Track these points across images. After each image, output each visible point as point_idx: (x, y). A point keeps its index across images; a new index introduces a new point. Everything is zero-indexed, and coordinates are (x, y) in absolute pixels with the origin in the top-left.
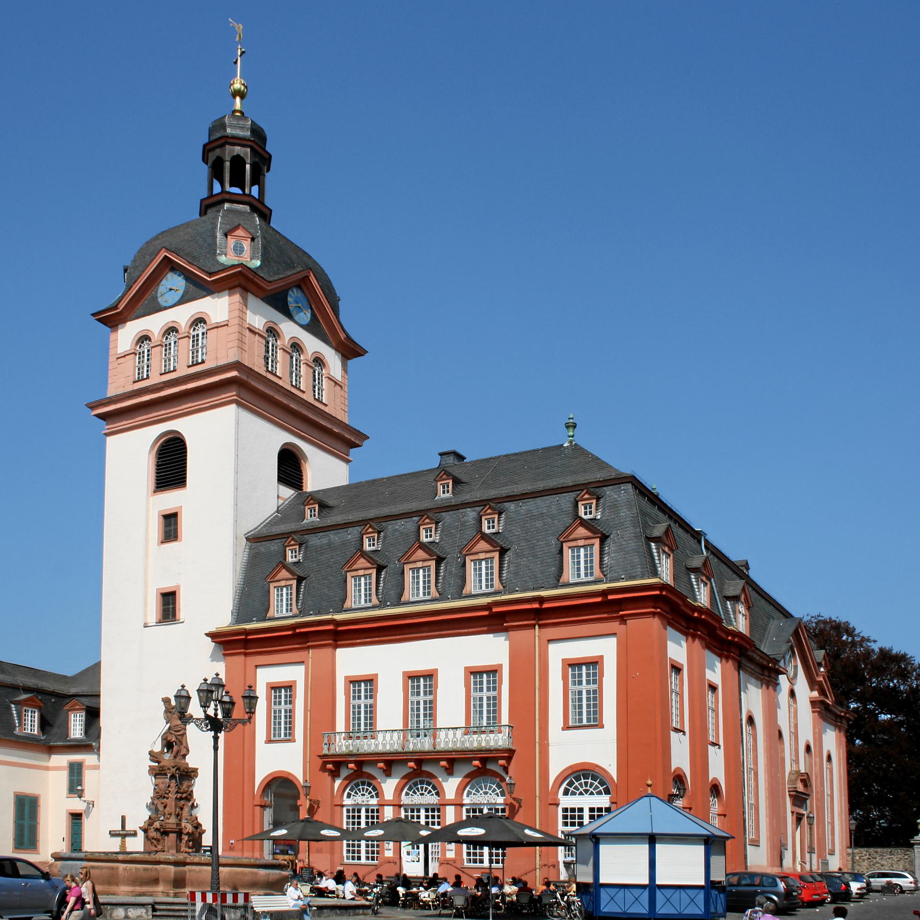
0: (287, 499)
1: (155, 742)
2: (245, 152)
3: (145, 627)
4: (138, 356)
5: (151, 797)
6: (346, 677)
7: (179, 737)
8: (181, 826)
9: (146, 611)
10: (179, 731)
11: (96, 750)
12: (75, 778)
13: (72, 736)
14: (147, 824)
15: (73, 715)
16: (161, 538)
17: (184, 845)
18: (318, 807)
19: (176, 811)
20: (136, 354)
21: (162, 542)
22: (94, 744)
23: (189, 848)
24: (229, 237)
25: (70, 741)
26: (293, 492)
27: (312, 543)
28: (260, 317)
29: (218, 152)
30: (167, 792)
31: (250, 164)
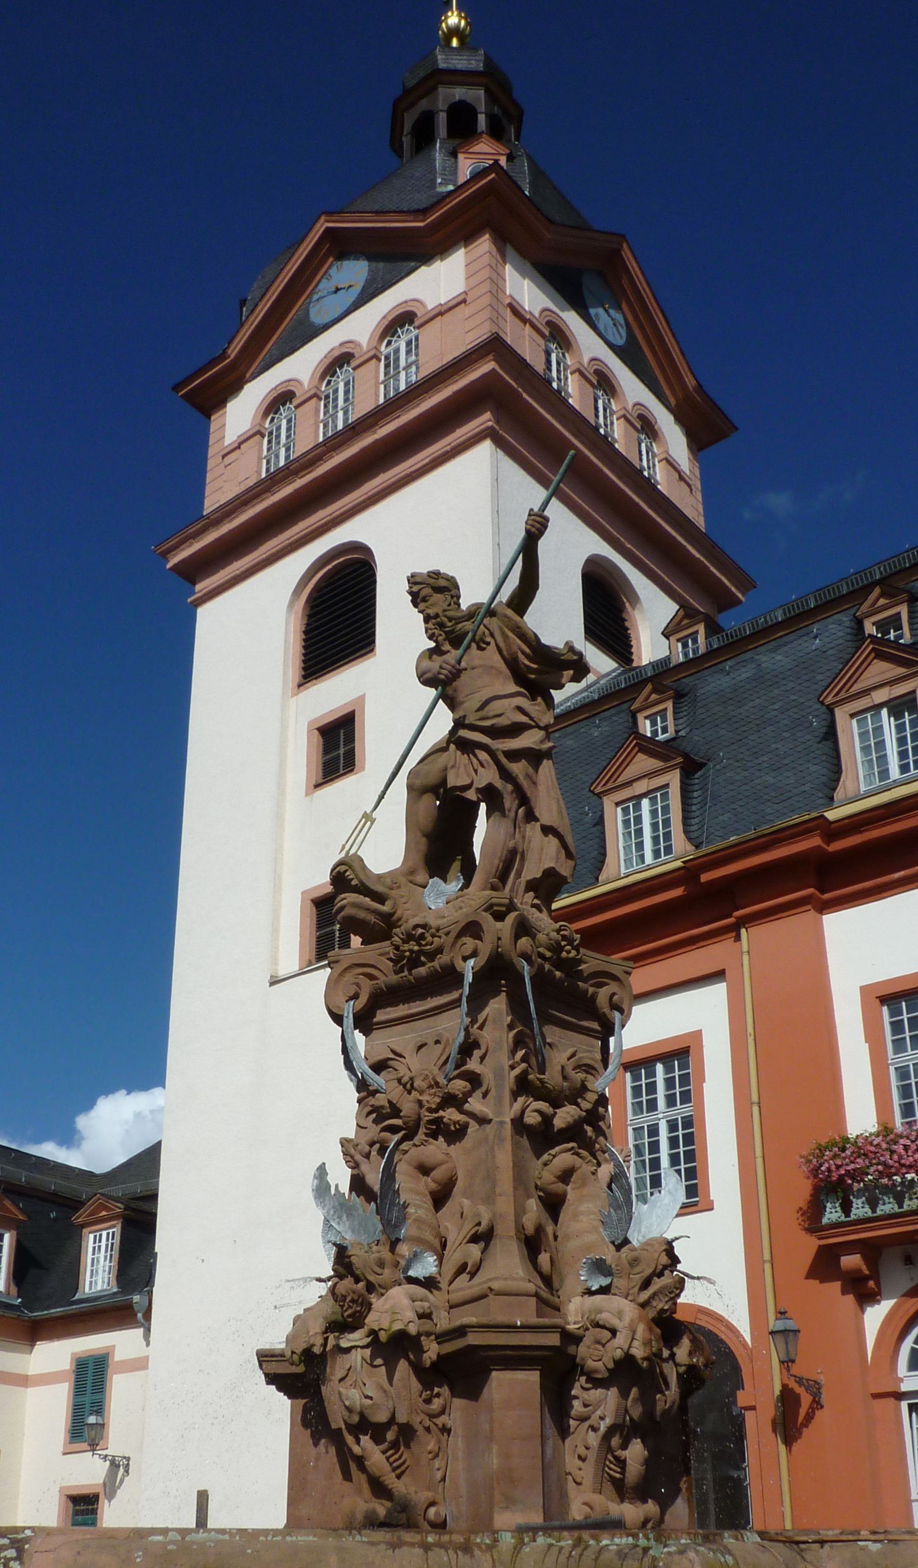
0: (604, 676)
1: (368, 818)
2: (477, 96)
3: (272, 984)
4: (266, 439)
5: (345, 1143)
6: (865, 990)
7: (518, 768)
8: (564, 1317)
9: (277, 948)
10: (515, 730)
11: (140, 1315)
12: (87, 1399)
13: (87, 1290)
14: (317, 1326)
15: (92, 1236)
16: (317, 776)
17: (587, 1473)
18: (817, 1404)
19: (519, 1212)
20: (263, 436)
21: (317, 786)
22: (136, 1298)
23: (621, 1490)
24: (461, 157)
25: (81, 1301)
26: (615, 665)
27: (702, 691)
28: (532, 284)
29: (423, 105)
30: (459, 1086)
31: (486, 114)
